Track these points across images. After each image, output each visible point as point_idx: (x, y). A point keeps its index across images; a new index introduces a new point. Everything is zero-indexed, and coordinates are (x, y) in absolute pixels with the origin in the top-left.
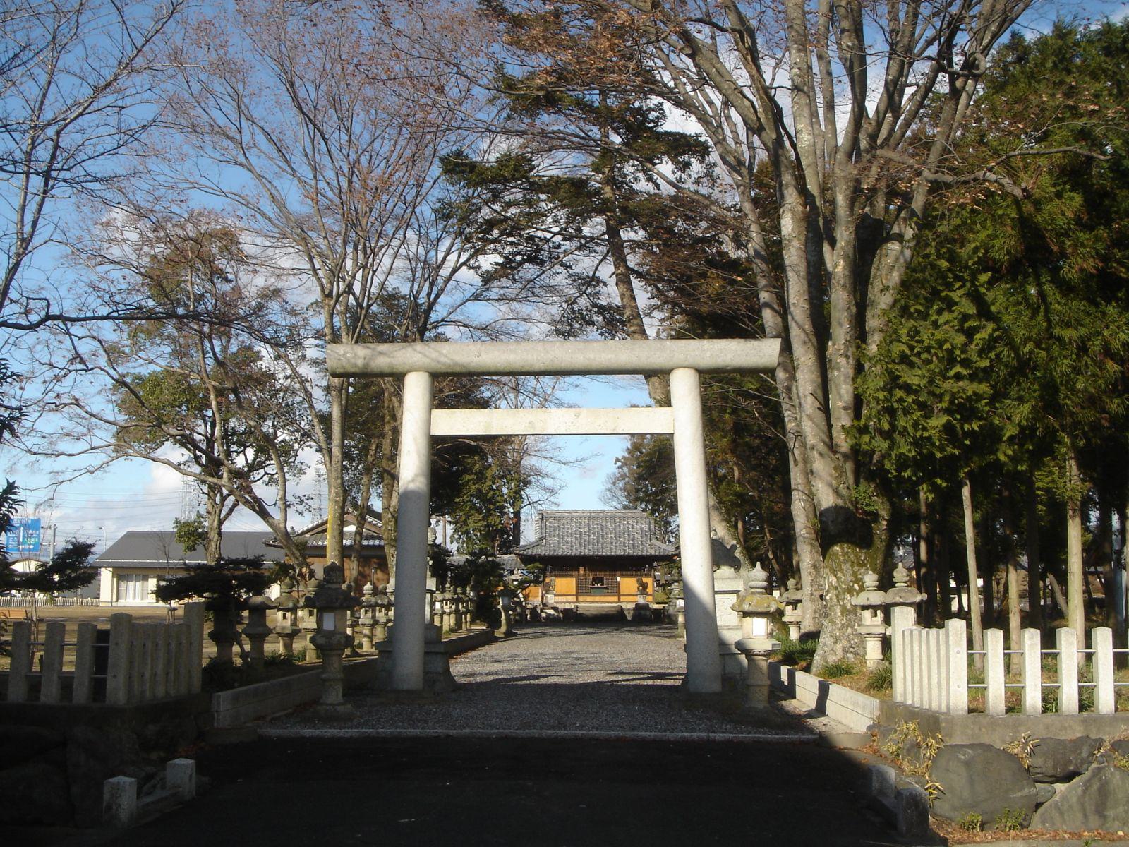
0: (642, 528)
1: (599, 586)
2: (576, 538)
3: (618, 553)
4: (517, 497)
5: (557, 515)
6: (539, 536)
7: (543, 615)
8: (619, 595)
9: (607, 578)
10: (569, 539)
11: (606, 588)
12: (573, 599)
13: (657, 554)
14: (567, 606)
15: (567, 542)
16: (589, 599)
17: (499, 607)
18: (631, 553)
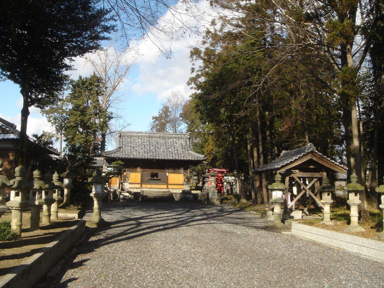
0: (182, 144)
1: (154, 177)
2: (142, 148)
3: (169, 158)
4: (104, 126)
5: (129, 134)
6: (118, 146)
7: (121, 196)
8: (168, 184)
9: (161, 173)
10: (138, 149)
11: (160, 180)
12: (139, 186)
13: (193, 159)
14: (136, 191)
15: (136, 150)
16: (149, 186)
17: (92, 195)
18: (177, 158)
